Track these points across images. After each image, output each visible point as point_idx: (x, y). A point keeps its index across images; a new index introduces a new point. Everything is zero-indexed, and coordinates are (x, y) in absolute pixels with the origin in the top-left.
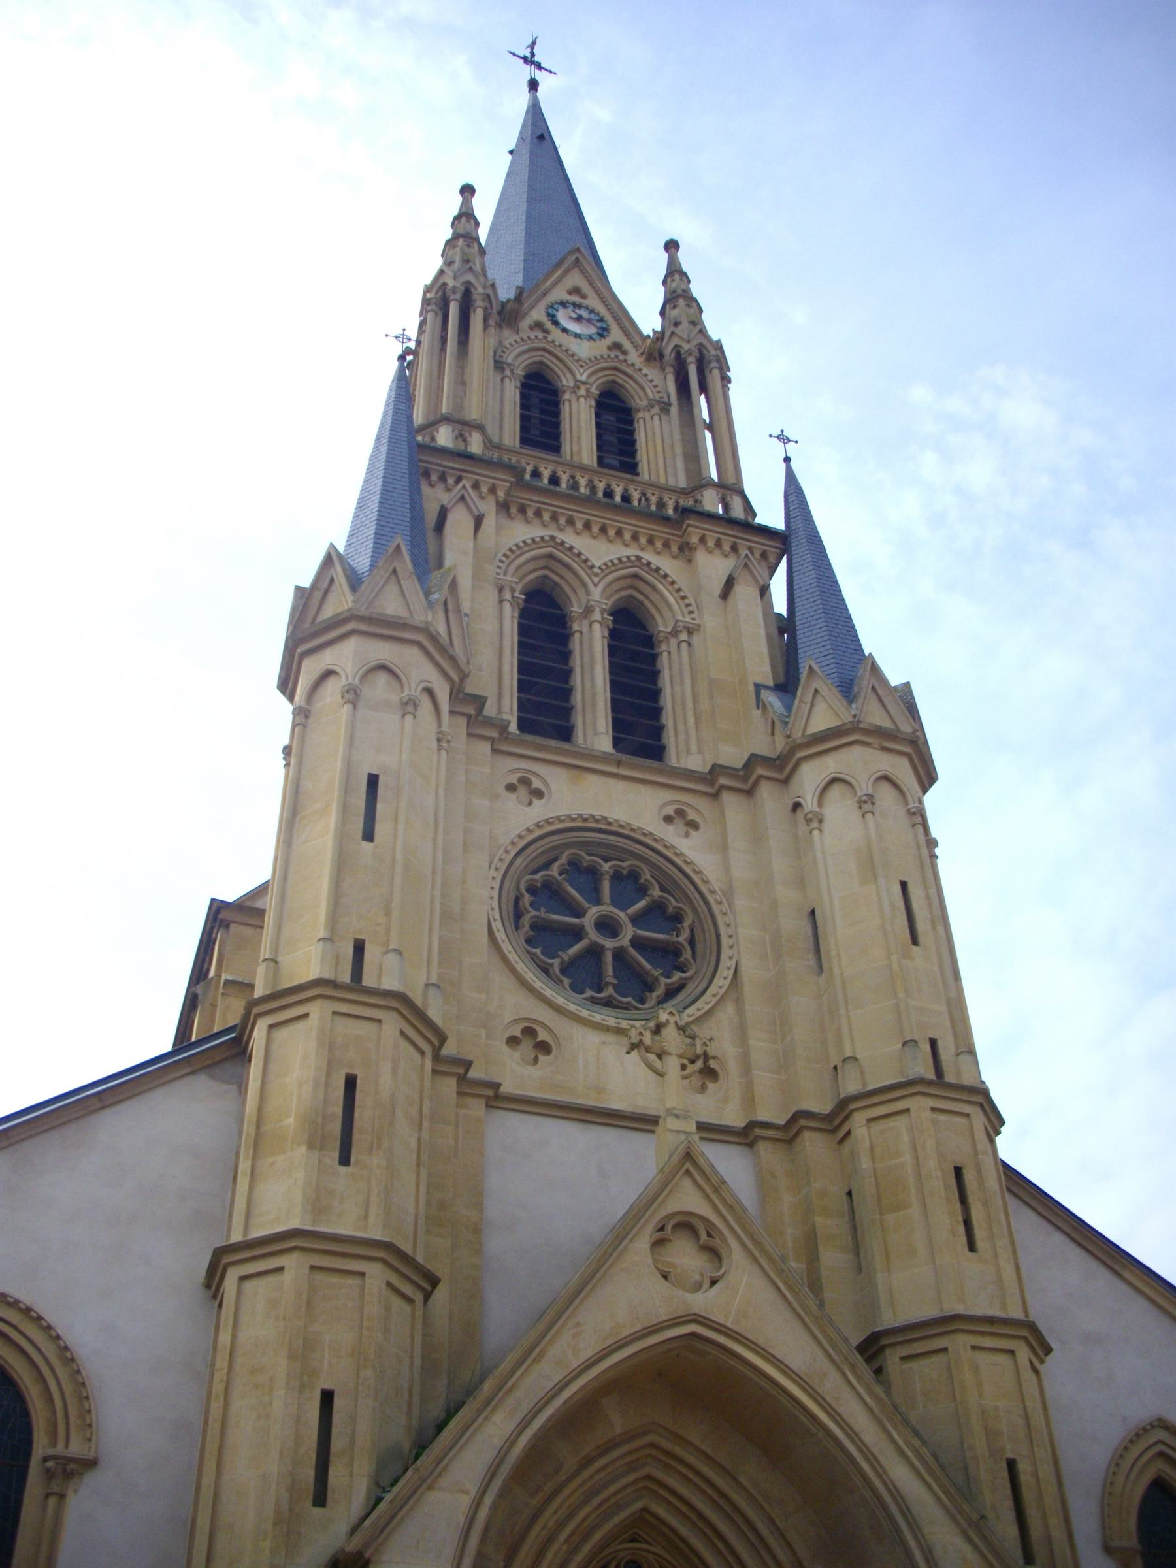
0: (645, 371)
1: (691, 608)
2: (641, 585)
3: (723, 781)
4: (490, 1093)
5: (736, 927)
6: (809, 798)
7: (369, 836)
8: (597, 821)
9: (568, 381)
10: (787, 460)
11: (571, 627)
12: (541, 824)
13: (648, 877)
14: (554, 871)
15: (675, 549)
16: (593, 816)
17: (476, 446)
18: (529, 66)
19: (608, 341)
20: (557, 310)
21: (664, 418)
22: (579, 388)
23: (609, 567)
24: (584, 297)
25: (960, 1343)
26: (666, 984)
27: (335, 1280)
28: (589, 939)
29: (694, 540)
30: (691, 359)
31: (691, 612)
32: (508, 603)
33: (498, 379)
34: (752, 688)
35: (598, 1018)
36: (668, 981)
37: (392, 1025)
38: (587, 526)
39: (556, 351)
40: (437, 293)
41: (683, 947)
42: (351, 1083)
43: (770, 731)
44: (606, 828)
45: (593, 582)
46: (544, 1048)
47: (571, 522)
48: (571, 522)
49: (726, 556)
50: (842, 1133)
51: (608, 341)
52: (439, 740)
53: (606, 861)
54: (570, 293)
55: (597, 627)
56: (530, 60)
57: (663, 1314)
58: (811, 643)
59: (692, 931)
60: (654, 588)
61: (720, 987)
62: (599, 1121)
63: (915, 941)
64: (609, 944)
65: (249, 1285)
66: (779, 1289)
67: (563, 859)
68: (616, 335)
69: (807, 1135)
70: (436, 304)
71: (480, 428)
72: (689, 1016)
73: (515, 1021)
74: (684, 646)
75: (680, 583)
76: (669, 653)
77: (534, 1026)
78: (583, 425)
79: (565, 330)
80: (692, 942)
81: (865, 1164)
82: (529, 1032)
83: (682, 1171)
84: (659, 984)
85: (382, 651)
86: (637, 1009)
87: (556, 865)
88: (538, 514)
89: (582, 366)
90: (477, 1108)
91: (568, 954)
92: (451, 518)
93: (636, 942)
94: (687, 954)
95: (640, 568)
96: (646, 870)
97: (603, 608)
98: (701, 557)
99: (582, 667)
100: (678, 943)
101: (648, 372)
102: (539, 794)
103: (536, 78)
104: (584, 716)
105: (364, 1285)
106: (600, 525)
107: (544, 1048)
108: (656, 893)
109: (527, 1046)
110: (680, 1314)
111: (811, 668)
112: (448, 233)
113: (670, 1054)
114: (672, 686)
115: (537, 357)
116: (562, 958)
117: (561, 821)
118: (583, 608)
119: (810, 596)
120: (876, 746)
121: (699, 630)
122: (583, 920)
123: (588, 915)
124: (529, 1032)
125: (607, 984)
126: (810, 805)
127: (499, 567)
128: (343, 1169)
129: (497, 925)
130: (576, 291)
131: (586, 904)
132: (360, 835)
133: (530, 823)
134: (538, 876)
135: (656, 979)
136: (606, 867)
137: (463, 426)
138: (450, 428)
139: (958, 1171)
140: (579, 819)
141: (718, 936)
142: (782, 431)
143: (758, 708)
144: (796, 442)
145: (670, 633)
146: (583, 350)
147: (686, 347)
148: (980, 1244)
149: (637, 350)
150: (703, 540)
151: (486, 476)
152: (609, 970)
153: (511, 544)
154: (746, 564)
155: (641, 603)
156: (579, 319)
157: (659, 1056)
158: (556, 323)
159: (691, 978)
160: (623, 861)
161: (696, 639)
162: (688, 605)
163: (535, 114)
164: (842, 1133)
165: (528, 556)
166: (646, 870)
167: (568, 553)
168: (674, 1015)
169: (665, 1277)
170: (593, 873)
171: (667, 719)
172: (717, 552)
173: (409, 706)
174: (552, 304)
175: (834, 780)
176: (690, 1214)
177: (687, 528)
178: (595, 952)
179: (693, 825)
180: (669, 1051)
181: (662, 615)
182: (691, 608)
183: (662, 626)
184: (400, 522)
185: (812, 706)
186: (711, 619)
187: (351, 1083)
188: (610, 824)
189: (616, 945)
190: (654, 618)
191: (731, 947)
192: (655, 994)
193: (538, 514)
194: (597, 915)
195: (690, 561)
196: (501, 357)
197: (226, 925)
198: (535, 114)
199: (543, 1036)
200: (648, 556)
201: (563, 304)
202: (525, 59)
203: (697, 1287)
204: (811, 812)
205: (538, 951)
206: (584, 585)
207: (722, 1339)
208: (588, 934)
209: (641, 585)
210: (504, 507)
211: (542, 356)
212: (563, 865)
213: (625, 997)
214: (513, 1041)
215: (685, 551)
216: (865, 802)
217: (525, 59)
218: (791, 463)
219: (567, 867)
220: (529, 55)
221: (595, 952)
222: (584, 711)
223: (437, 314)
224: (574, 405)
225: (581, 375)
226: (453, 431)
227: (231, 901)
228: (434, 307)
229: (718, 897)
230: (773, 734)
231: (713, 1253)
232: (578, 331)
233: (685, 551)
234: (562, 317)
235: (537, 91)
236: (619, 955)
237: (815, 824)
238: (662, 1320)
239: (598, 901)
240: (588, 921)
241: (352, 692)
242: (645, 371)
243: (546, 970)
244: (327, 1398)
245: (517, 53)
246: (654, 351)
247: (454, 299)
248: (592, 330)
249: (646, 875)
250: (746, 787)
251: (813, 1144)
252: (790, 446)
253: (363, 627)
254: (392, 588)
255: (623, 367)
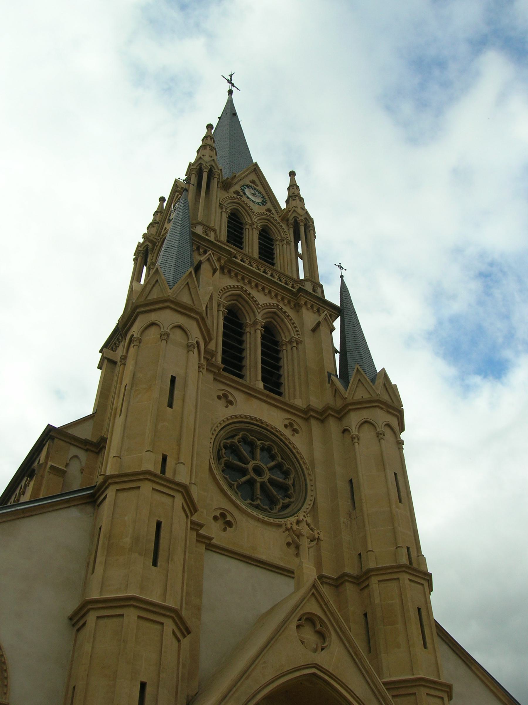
0: (281, 224)
1: (298, 333)
2: (276, 318)
3: (312, 413)
4: (208, 542)
5: (315, 482)
6: (353, 428)
7: (170, 405)
8: (257, 421)
9: (248, 220)
10: (342, 277)
11: (245, 330)
12: (233, 417)
13: (276, 451)
14: (236, 440)
15: (292, 305)
16: (255, 418)
17: (212, 238)
18: (229, 84)
19: (266, 207)
20: (245, 188)
21: (288, 246)
22: (254, 224)
23: (266, 306)
24: (257, 185)
25: (423, 691)
26: (283, 503)
27: (148, 624)
28: (250, 475)
29: (303, 302)
30: (302, 224)
31: (298, 334)
32: (222, 312)
33: (220, 211)
34: (326, 374)
35: (255, 514)
36: (283, 501)
37: (179, 500)
38: (257, 286)
39: (245, 206)
40: (197, 167)
41: (290, 486)
42: (159, 525)
43: (333, 394)
44: (260, 424)
45: (258, 311)
46: (229, 524)
47: (250, 282)
48: (250, 282)
49: (314, 313)
50: (364, 585)
51: (266, 207)
52: (199, 367)
53: (259, 440)
54: (251, 182)
55: (258, 331)
56: (230, 82)
57: (302, 663)
58: (354, 358)
59: (294, 479)
60: (282, 320)
61: (307, 509)
62: (254, 563)
63: (400, 501)
64: (259, 479)
65: (102, 622)
66: (352, 657)
67: (240, 435)
68: (269, 205)
69: (347, 584)
70: (196, 171)
71: (214, 230)
72: (279, 521)
73: (217, 509)
74: (295, 348)
75: (295, 320)
76: (287, 351)
77: (226, 513)
78: (255, 241)
79: (248, 198)
80: (293, 485)
81: (377, 601)
82: (223, 515)
83: (310, 594)
84: (279, 503)
85: (181, 320)
86: (270, 512)
87: (237, 438)
88: (236, 275)
89: (255, 215)
90: (202, 548)
91: (241, 481)
92: (203, 266)
93: (271, 481)
94: (291, 491)
95: (278, 310)
96: (276, 448)
97: (262, 324)
98: (304, 310)
99: (250, 349)
100: (288, 484)
101: (282, 225)
102: (231, 403)
103: (232, 89)
104: (250, 371)
105: (163, 629)
106: (262, 286)
107: (229, 524)
108: (280, 459)
109: (220, 522)
110: (310, 663)
111: (358, 369)
112: (200, 143)
113: (304, 535)
114: (287, 366)
115: (235, 206)
116: (238, 482)
117: (242, 418)
118: (252, 322)
119: (354, 338)
120: (385, 409)
121: (301, 343)
122: (248, 466)
123: (251, 464)
124: (223, 515)
125: (257, 498)
126: (354, 431)
127: (218, 295)
128: (154, 568)
129: (212, 461)
130: (253, 182)
131: (249, 459)
132: (166, 404)
133: (228, 416)
134: (229, 441)
135: (278, 500)
136: (259, 443)
137: (208, 228)
138: (202, 227)
139: (419, 609)
140: (249, 418)
141: (306, 485)
142: (340, 264)
143: (329, 383)
144: (346, 270)
145: (288, 342)
146: (256, 209)
147: (300, 218)
148: (429, 645)
149: (278, 214)
150: (306, 303)
151: (218, 253)
152: (259, 492)
153: (224, 286)
154: (325, 318)
155: (275, 326)
156: (254, 195)
157: (298, 537)
158: (245, 194)
159: (293, 502)
160: (266, 442)
161: (300, 346)
162: (297, 331)
163: (230, 105)
164: (364, 585)
165: (230, 293)
166: (276, 448)
167: (248, 296)
168: (305, 517)
169: (303, 642)
170: (252, 445)
171: (284, 381)
172: (311, 310)
173: (189, 347)
174: (244, 185)
175: (366, 422)
176: (312, 613)
177: (300, 297)
178: (251, 483)
179: (295, 431)
180: (304, 534)
181: (284, 333)
182: (298, 333)
183: (285, 338)
184: (186, 263)
185: (357, 387)
186: (308, 341)
187: (159, 525)
188: (262, 423)
189: (262, 480)
190: (280, 333)
191: (312, 491)
192: (278, 507)
193: (236, 275)
194: (254, 465)
195: (298, 312)
196: (222, 202)
197: (53, 438)
198: (230, 105)
199: (229, 518)
200: (281, 305)
201: (248, 187)
202: (228, 80)
203: (315, 651)
204: (355, 434)
205: (227, 477)
206: (254, 312)
207: (327, 678)
208: (250, 473)
209: (276, 318)
210: (222, 268)
211: (238, 206)
212: (240, 438)
213: (265, 506)
214: (215, 518)
215: (297, 307)
216: (381, 434)
217: (228, 80)
218: (343, 278)
219: (241, 439)
220: (230, 79)
221: (251, 483)
222: (250, 369)
223: (196, 176)
224: (251, 231)
225: (255, 219)
226: (203, 229)
227: (57, 427)
228: (195, 172)
229: (307, 466)
230: (335, 396)
231: (322, 635)
232: (254, 200)
233: (297, 307)
234: (247, 191)
235: (232, 95)
236: (263, 485)
237: (356, 440)
238: (301, 665)
239: (253, 458)
240: (250, 466)
241: (166, 335)
242: (281, 224)
243: (231, 486)
244: (143, 685)
245: (225, 77)
246: (284, 216)
247: (205, 171)
248: (259, 200)
249: (275, 450)
250: (339, 417)
251: (349, 589)
252: (342, 270)
253: (173, 306)
254: (186, 291)
255: (272, 220)
